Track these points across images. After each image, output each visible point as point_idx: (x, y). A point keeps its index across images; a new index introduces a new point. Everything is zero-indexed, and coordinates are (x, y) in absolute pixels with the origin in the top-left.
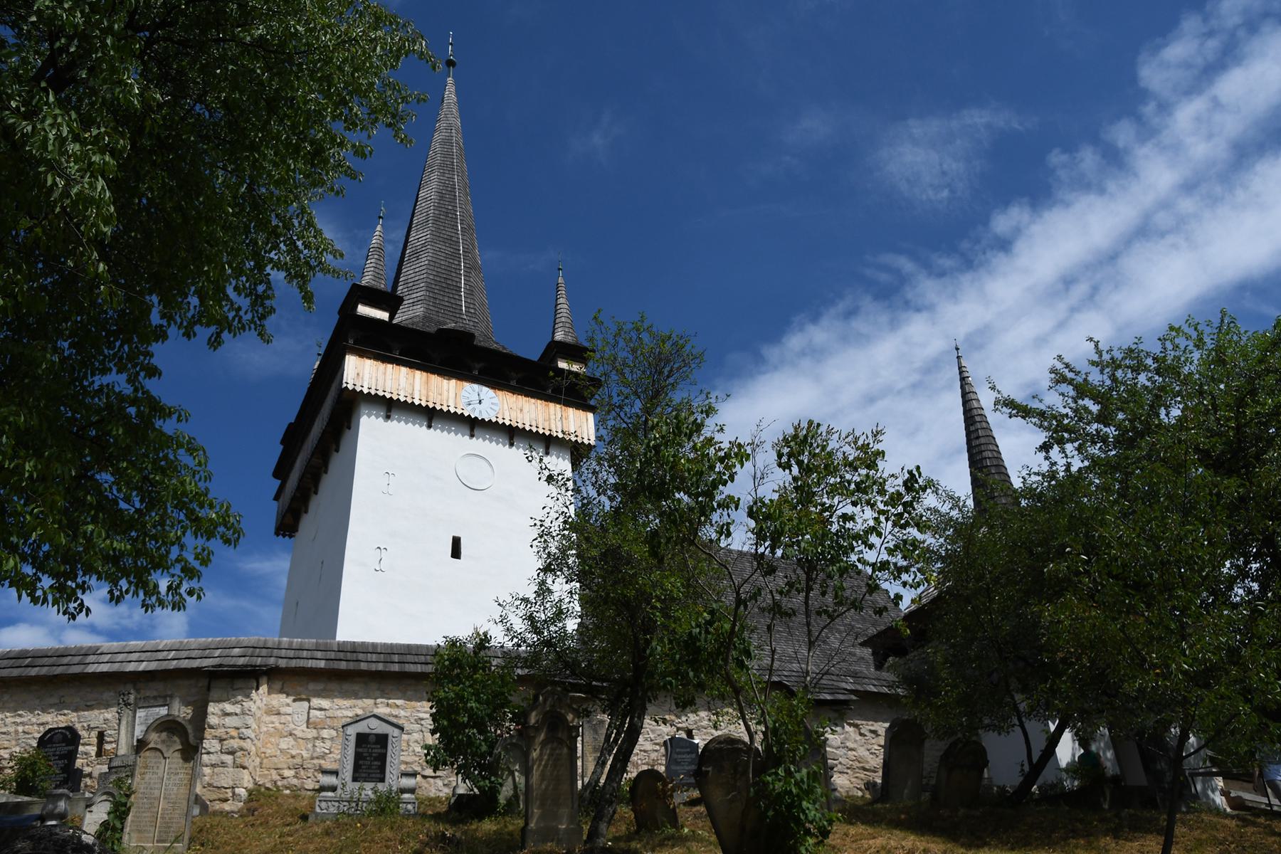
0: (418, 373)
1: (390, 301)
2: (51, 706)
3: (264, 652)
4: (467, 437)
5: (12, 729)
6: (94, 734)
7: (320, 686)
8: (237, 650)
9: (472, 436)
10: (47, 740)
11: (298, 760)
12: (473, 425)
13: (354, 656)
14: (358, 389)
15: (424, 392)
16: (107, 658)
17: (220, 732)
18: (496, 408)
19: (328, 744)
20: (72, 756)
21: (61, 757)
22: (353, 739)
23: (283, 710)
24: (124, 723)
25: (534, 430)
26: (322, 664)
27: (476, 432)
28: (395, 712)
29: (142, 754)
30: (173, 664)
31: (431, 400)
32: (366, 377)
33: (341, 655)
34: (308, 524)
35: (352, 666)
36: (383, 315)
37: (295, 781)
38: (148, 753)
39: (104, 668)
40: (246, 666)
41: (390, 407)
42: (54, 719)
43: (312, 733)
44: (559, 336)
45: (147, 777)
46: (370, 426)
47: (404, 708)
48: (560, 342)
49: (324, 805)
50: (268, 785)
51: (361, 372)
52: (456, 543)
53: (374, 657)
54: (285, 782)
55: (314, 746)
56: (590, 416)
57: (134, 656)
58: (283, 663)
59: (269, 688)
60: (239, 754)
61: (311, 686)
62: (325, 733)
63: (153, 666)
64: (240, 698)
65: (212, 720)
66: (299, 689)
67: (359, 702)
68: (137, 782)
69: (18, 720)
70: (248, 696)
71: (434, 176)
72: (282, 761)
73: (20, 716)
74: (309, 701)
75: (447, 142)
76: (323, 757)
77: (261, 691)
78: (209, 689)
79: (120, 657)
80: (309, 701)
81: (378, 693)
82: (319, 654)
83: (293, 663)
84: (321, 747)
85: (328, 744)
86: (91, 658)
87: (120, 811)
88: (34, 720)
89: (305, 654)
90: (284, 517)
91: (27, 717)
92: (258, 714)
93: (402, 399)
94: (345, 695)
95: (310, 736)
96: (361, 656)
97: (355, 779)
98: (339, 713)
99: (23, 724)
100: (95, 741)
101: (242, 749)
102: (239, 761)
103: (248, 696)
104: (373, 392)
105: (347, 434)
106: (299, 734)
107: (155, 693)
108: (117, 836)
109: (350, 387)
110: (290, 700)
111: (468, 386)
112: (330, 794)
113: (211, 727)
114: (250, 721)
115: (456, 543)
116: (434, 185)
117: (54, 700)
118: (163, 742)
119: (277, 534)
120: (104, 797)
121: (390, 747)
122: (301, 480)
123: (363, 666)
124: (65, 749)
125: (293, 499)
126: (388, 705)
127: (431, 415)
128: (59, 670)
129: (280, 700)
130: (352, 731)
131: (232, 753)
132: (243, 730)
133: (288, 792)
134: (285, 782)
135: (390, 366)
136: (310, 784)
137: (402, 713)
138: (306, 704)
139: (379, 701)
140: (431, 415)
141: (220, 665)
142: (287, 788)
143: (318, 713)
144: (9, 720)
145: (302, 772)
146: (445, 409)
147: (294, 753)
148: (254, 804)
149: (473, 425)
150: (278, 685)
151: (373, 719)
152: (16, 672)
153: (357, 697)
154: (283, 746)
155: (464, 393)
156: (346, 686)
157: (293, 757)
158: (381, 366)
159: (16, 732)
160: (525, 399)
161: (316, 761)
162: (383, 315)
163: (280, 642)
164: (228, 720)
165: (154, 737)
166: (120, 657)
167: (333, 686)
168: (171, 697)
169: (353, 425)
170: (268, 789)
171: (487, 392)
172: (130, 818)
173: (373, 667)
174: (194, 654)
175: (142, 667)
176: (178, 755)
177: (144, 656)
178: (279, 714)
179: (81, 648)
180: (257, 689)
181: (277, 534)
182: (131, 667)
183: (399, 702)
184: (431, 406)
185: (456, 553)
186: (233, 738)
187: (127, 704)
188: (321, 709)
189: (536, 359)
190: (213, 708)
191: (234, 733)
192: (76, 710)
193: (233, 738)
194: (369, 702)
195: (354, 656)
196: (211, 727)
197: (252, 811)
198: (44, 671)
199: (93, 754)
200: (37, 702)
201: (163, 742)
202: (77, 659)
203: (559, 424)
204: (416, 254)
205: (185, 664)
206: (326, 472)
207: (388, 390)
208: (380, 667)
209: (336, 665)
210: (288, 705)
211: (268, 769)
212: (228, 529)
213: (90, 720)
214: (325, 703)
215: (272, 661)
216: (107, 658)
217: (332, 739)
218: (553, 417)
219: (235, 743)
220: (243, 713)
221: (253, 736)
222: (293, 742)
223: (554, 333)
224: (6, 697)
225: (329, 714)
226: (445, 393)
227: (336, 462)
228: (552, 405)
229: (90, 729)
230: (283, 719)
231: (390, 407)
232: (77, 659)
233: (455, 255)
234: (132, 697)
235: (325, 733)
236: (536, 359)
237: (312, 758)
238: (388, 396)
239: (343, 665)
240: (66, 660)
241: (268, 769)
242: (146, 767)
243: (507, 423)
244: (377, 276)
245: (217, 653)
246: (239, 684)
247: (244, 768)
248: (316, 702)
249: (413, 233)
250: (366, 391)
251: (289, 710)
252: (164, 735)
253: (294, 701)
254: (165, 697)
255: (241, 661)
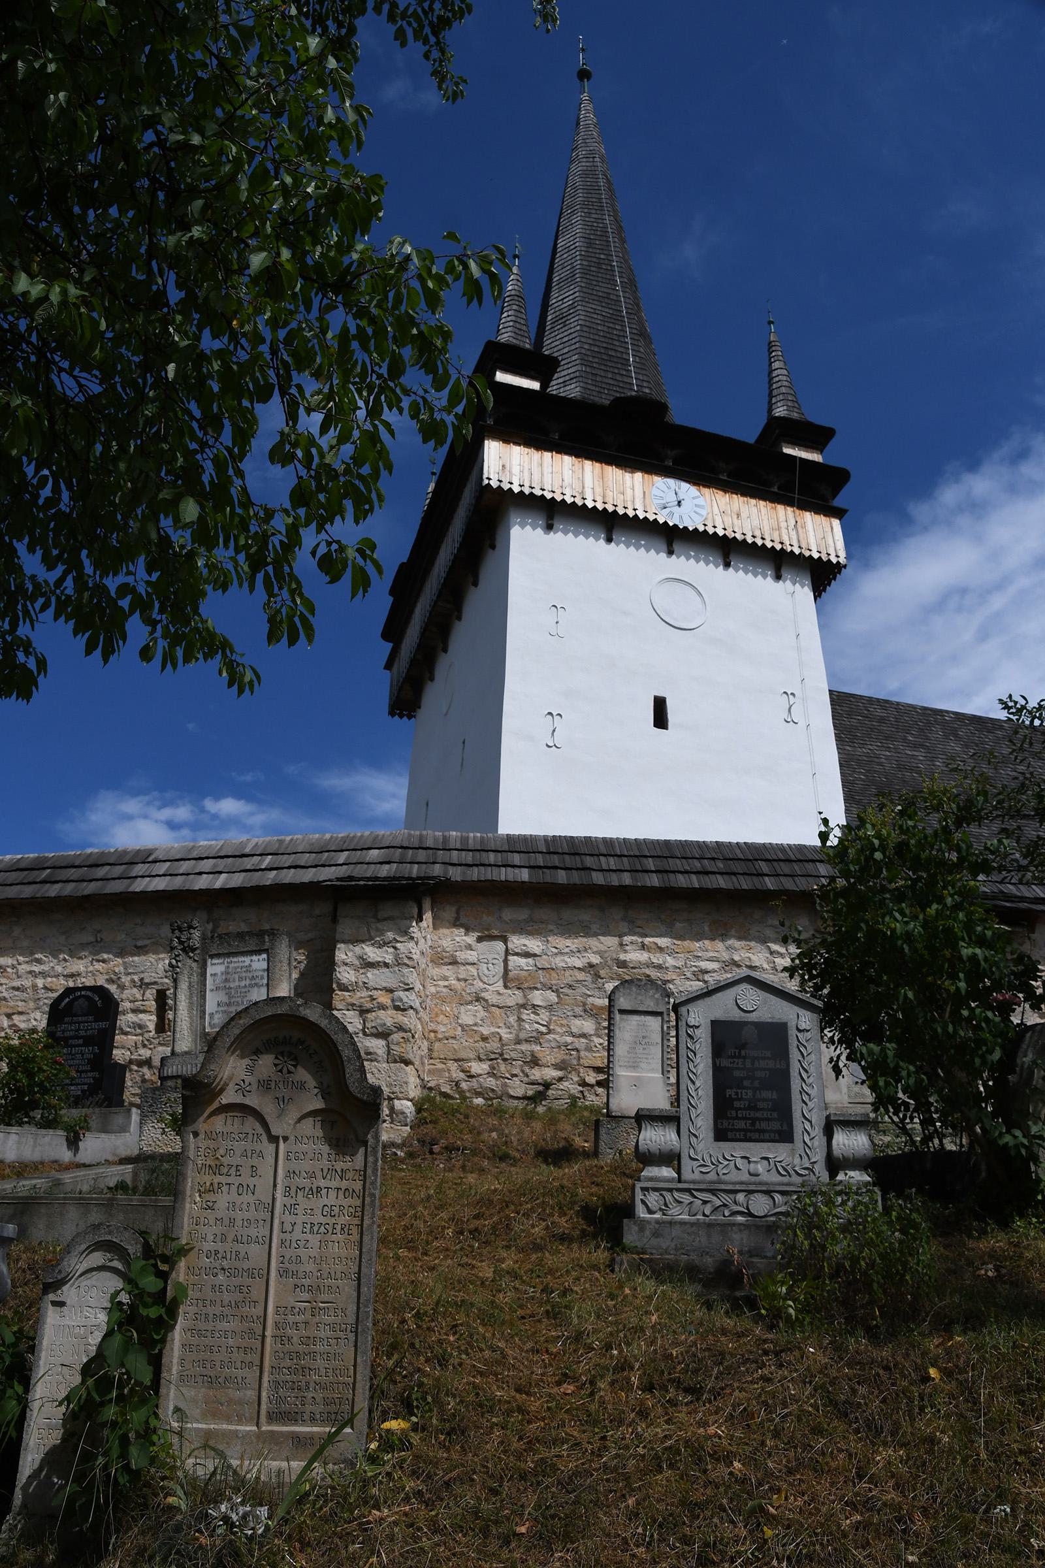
0: (588, 463)
1: (543, 366)
2: (83, 946)
3: (422, 855)
4: (663, 555)
5: (27, 983)
6: (151, 994)
7: (522, 914)
8: (374, 854)
9: (670, 552)
10: (66, 1008)
11: (494, 1045)
12: (672, 538)
13: (577, 861)
14: (506, 487)
15: (599, 490)
16: (163, 868)
17: (361, 996)
18: (704, 512)
19: (544, 1016)
20: (105, 1040)
21: (88, 1041)
22: (704, 1036)
23: (462, 956)
24: (183, 986)
25: (759, 542)
26: (524, 875)
27: (676, 547)
28: (657, 959)
29: (201, 1125)
30: (270, 877)
31: (610, 500)
32: (516, 470)
33: (555, 860)
34: (434, 696)
35: (576, 878)
36: (535, 385)
37: (491, 1082)
38: (219, 1123)
39: (160, 884)
40: (394, 878)
41: (553, 512)
42: (88, 970)
43: (513, 997)
44: (780, 411)
45: (222, 1200)
46: (525, 541)
47: (672, 953)
48: (779, 418)
49: (653, 1199)
50: (446, 1089)
51: (507, 464)
52: (660, 705)
53: (612, 863)
54: (474, 1083)
55: (520, 1020)
56: (836, 523)
57: (207, 865)
58: (455, 874)
59: (435, 918)
60: (396, 1037)
61: (508, 914)
62: (537, 997)
63: (237, 880)
64: (390, 935)
65: (345, 975)
66: (486, 919)
67: (593, 942)
68: (194, 1217)
69: (37, 968)
70: (405, 932)
71: (577, 218)
72: (465, 1046)
73: (39, 961)
74: (505, 940)
75: (590, 173)
76: (537, 1039)
77: (424, 924)
78: (334, 919)
79: (185, 867)
80: (505, 940)
81: (624, 926)
82: (516, 859)
83: (475, 874)
84: (532, 1022)
85: (544, 1016)
86: (140, 869)
87: (142, 1323)
88: (59, 969)
89: (492, 858)
90: (400, 689)
91: (49, 964)
92: (423, 963)
93: (569, 500)
94: (568, 930)
95: (511, 1002)
96: (589, 861)
97: (721, 1135)
98: (559, 962)
99: (43, 974)
100: (152, 1005)
101: (400, 1028)
102: (397, 1050)
103: (405, 932)
104: (527, 491)
105: (491, 558)
106: (493, 998)
107: (244, 928)
108: (137, 1417)
109: (494, 484)
110: (471, 939)
111: (659, 481)
112: (667, 1172)
113: (344, 988)
114: (413, 978)
115: (660, 705)
116: (578, 229)
117: (88, 937)
118: (265, 1086)
119: (392, 713)
120: (97, 1258)
121: (794, 1055)
122: (424, 634)
123: (598, 878)
124: (94, 1027)
125: (413, 663)
126: (643, 947)
127: (610, 524)
128: (90, 888)
129: (454, 939)
130: (699, 1016)
131: (384, 1035)
132: (401, 994)
133: (479, 1101)
134: (474, 1083)
135: (547, 455)
136: (518, 1088)
137: (670, 961)
138: (499, 946)
139: (627, 939)
140: (610, 524)
141: (351, 878)
142: (478, 1094)
143: (522, 961)
144: (24, 968)
145: (503, 1067)
146: (631, 514)
147: (485, 1031)
148: (428, 1129)
149: (672, 538)
150: (449, 913)
151: (744, 986)
152: (27, 892)
153: (587, 934)
154: (467, 1019)
155: (655, 491)
156: (568, 914)
157: (484, 1039)
158: (535, 455)
159: (34, 986)
160: (742, 499)
161: (524, 1047)
162: (535, 385)
163: (446, 839)
164: (372, 976)
165: (235, 1072)
166: (185, 867)
167: (545, 913)
168: (273, 933)
169: (498, 544)
170: (445, 1095)
171: (687, 490)
172: (178, 1335)
173: (614, 880)
174: (304, 859)
175: (220, 882)
176: (310, 1128)
177: (222, 864)
178: (454, 963)
179: (125, 852)
180: (420, 919)
181: (392, 713)
182: (202, 883)
183: (663, 942)
184: (610, 509)
185: (661, 719)
186: (383, 1007)
187: (188, 949)
188: (527, 955)
189: (751, 439)
190: (343, 953)
191: (384, 999)
192: (121, 954)
193: (383, 1007)
194: (610, 942)
195: (577, 861)
196: (344, 988)
197: (427, 1144)
198: (68, 889)
199: (152, 1027)
200: (62, 939)
201: (265, 1086)
202: (118, 870)
203: (793, 534)
204: (562, 319)
205: (289, 876)
206: (459, 618)
207: (548, 487)
208: (627, 879)
209: (548, 877)
210: (469, 947)
211: (444, 1060)
212: (439, 385)
213: (131, 975)
214: (534, 944)
215: (437, 870)
216: (163, 868)
217: (550, 1007)
218: (783, 525)
219: (388, 1018)
220: (399, 963)
221: (417, 1005)
222: (482, 1014)
223: (770, 410)
224: (17, 931)
225: (542, 962)
226: (629, 492)
227: (475, 602)
228: (780, 508)
229: (143, 985)
230: (462, 971)
231: (553, 512)
232: (118, 870)
233: (617, 317)
234: (196, 935)
235: (537, 997)
236: (751, 439)
237: (518, 1042)
238: (549, 496)
239: (562, 877)
240: (101, 872)
241: (444, 1060)
242: (216, 1169)
243: (721, 533)
244: (518, 333)
245: (342, 857)
246: (387, 910)
247: (407, 1063)
248: (517, 942)
249: (554, 294)
250: (516, 489)
251: (471, 956)
252: (266, 1062)
253: (480, 940)
254: (260, 934)
255: (385, 871)
